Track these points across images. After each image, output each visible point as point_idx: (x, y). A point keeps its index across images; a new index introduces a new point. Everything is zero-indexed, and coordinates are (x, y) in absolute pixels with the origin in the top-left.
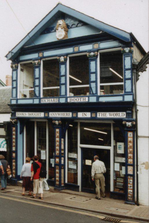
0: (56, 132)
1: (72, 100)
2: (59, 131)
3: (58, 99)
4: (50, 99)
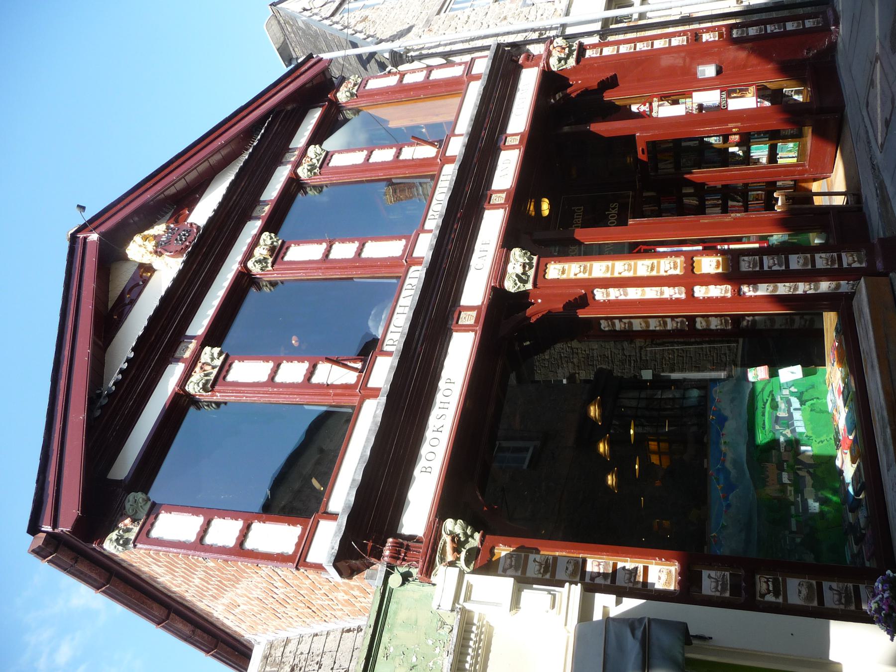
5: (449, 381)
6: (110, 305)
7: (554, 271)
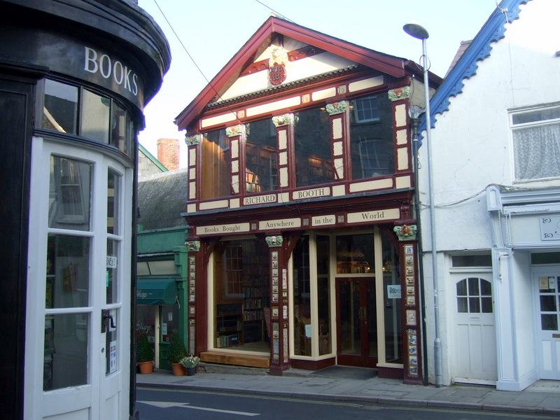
7: (275, 254)
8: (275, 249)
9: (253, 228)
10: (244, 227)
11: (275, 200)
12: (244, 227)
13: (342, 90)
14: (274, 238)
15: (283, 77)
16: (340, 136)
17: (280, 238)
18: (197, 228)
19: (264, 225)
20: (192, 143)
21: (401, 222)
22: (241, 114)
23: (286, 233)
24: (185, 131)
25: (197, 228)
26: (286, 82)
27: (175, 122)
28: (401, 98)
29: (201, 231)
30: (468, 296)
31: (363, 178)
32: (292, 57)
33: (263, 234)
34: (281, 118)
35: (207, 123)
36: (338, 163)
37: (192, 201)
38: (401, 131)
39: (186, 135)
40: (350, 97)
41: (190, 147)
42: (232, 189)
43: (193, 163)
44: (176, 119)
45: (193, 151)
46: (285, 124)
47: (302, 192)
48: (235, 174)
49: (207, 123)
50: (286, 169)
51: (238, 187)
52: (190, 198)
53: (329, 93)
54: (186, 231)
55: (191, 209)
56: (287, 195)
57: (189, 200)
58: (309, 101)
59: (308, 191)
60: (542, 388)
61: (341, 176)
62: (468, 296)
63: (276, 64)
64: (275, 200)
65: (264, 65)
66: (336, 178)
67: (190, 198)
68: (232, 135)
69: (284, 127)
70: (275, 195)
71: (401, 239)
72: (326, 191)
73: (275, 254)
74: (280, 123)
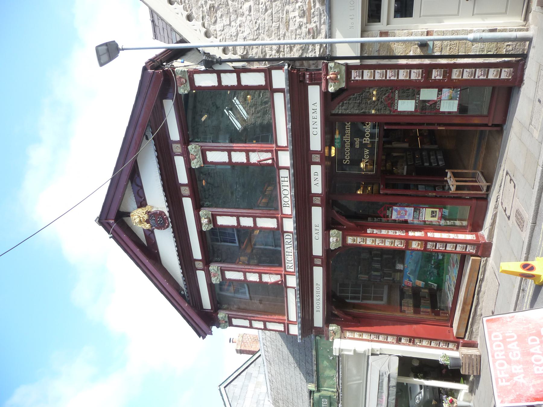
0: (355, 243)
1: (286, 203)
2: (351, 238)
3: (285, 234)
4: (286, 250)
5: (315, 174)
6: (145, 243)
7: (350, 240)
8: (344, 240)
9: (320, 263)
10: (318, 273)
11: (291, 235)
12: (318, 273)
13: (199, 265)
14: (332, 240)
15: (161, 213)
16: (226, 153)
17: (332, 232)
18: (315, 325)
19: (317, 249)
20: (226, 322)
21: (323, 84)
22: (177, 148)
23: (329, 225)
24: (214, 328)
25: (315, 325)
26: (166, 210)
27: (204, 338)
28: (187, 79)
29: (318, 320)
30: (372, 295)
31: (269, 143)
32: (142, 203)
33: (327, 251)
34: (204, 221)
35: (207, 303)
36: (255, 158)
37: (287, 329)
38: (232, 157)
39: (218, 327)
40: (186, 141)
41: (231, 324)
42: (276, 283)
43: (246, 323)
44: (199, 335)
45: (235, 321)
46: (210, 216)
47: (283, 203)
48: (260, 278)
49: (207, 303)
50: (258, 220)
51: (275, 276)
52: (283, 330)
53: (179, 162)
54: (318, 338)
55: (294, 330)
56: (285, 220)
57: (285, 331)
58: (187, 188)
59: (283, 196)
60: (530, 9)
61: (269, 155)
62: (372, 295)
63: (147, 221)
64: (291, 235)
65: (149, 235)
66: (270, 162)
67: (283, 330)
68: (220, 277)
69: (213, 220)
70: (285, 234)
71: (343, 85)
72: (284, 174)
73: (350, 240)
74: (209, 222)
